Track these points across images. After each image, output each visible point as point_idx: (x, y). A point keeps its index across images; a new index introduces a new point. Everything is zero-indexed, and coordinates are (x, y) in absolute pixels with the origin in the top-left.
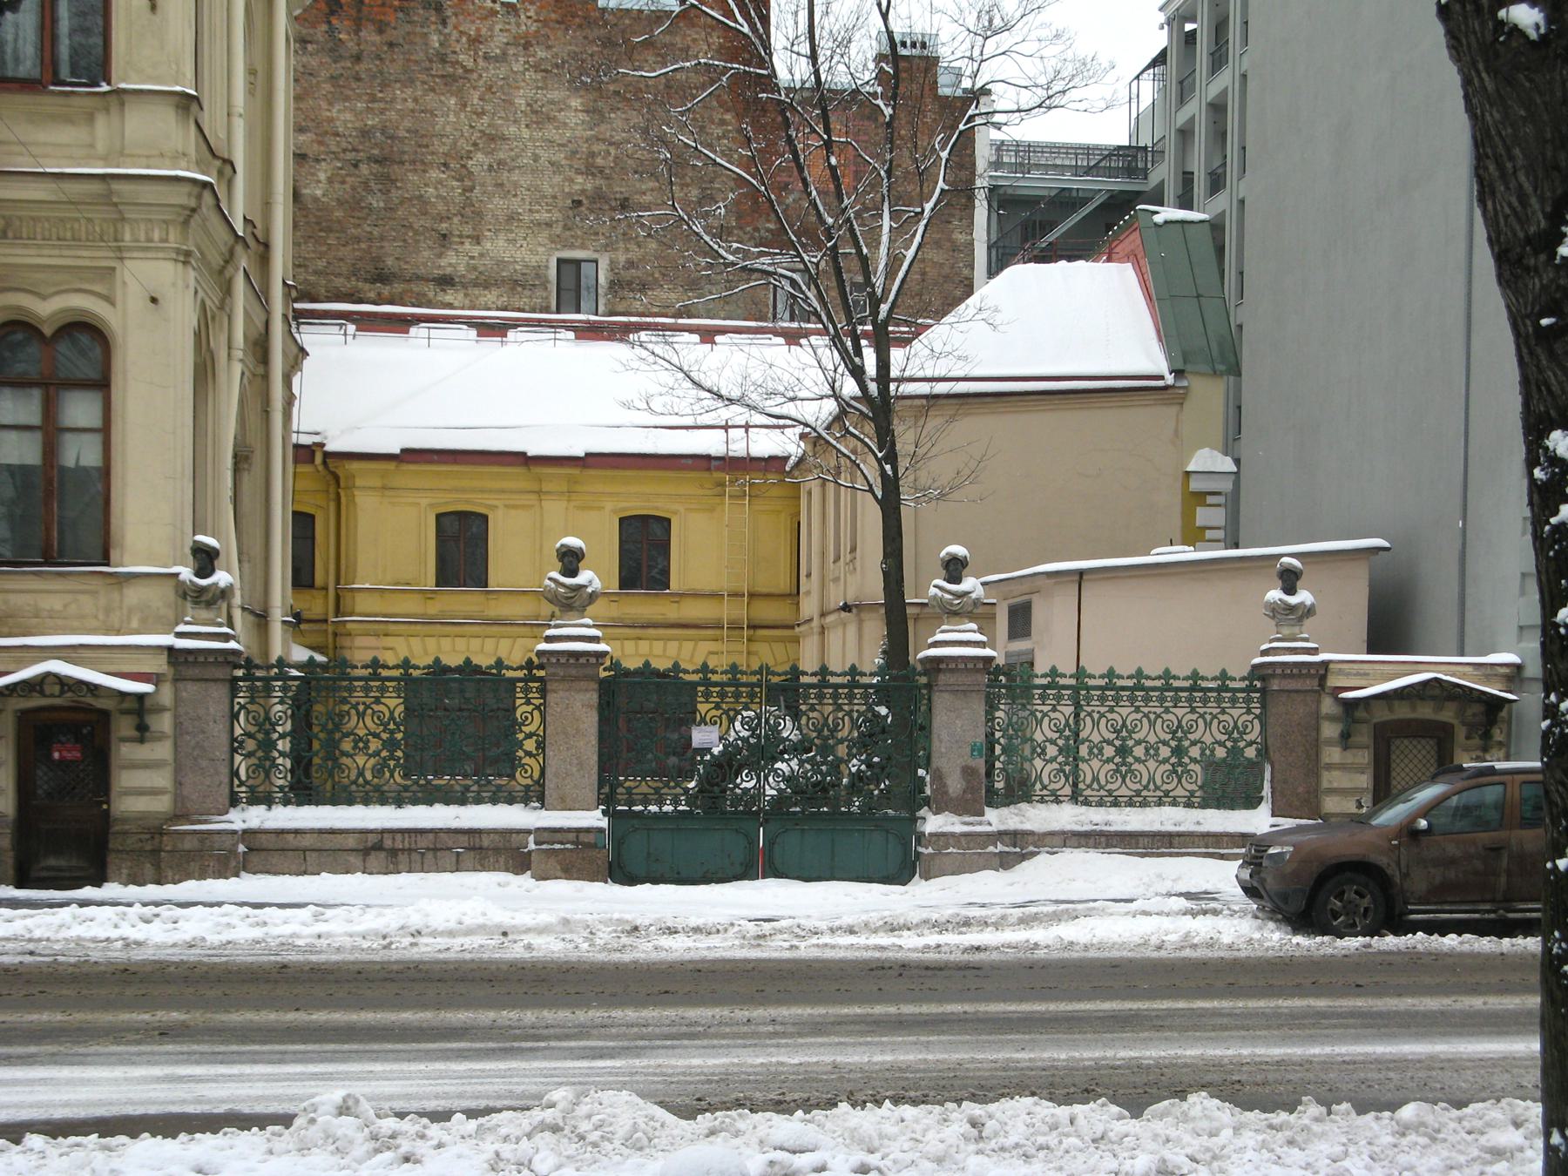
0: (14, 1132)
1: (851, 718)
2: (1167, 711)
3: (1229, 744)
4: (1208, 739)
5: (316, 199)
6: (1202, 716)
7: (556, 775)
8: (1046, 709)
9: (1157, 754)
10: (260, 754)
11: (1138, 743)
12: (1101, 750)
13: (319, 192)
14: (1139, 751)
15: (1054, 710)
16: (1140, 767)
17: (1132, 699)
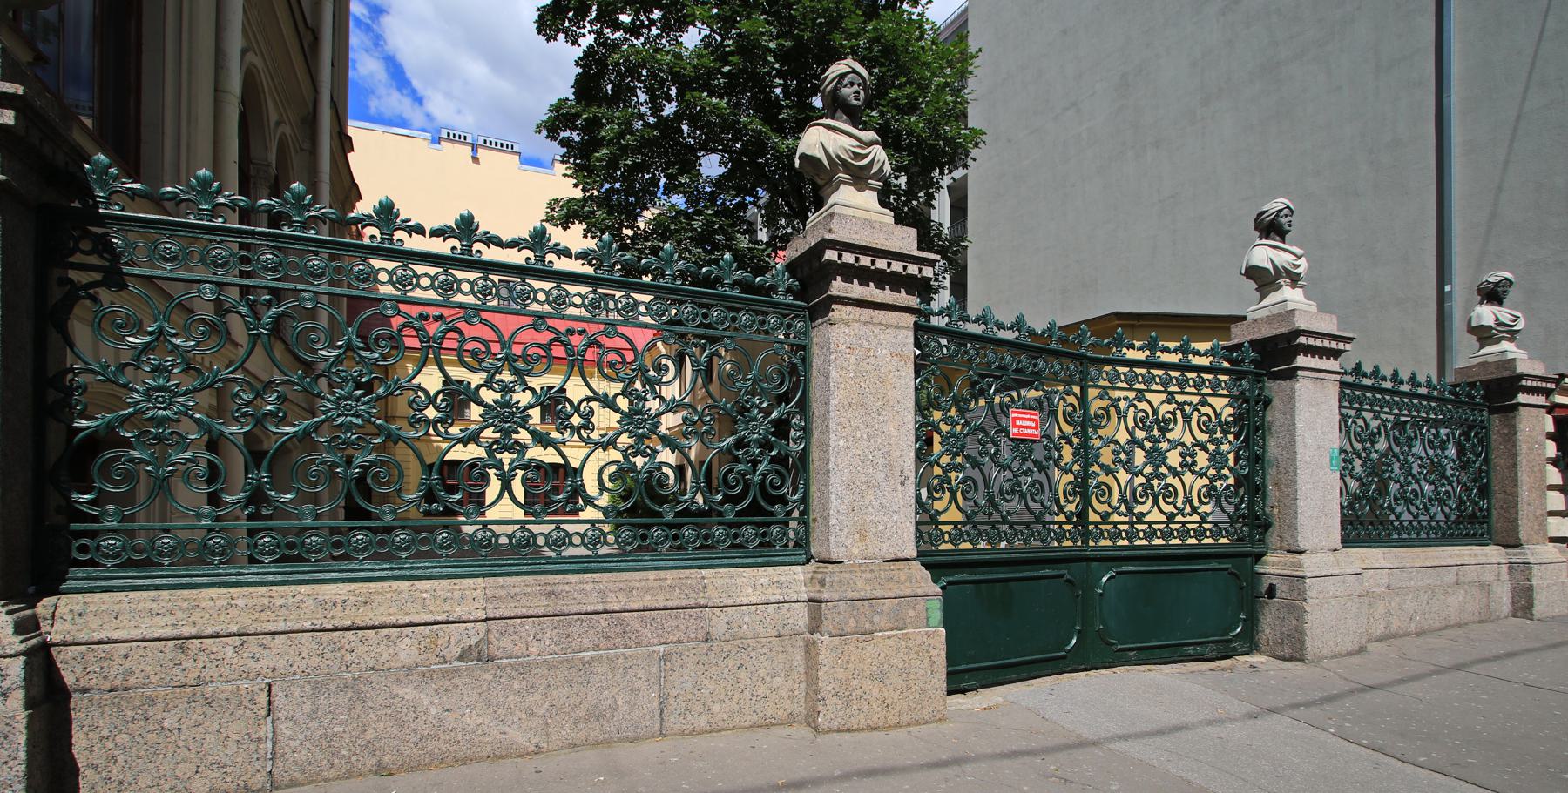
9: (588, 426)
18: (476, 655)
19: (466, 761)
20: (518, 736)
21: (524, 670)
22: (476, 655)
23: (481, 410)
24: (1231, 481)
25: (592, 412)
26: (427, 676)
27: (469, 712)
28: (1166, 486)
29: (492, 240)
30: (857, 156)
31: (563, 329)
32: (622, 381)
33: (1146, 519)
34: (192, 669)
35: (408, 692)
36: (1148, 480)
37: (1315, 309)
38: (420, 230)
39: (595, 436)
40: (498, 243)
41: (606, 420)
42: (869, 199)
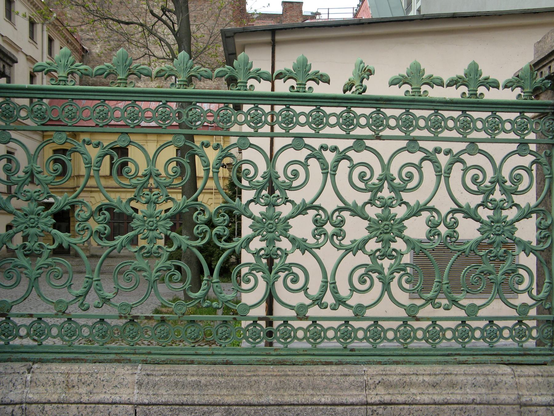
1: (335, 292)
2: (360, 144)
3: (485, 213)
4: (443, 204)
5: (96, 53)
9: (340, 234)
11: (303, 209)
13: (97, 51)
14: (356, 228)
16: (307, 260)
23: (250, 221)
24: (407, 259)
25: (456, 223)
29: (433, 82)
31: (431, 150)
32: (483, 193)
33: (369, 313)
38: (496, 85)
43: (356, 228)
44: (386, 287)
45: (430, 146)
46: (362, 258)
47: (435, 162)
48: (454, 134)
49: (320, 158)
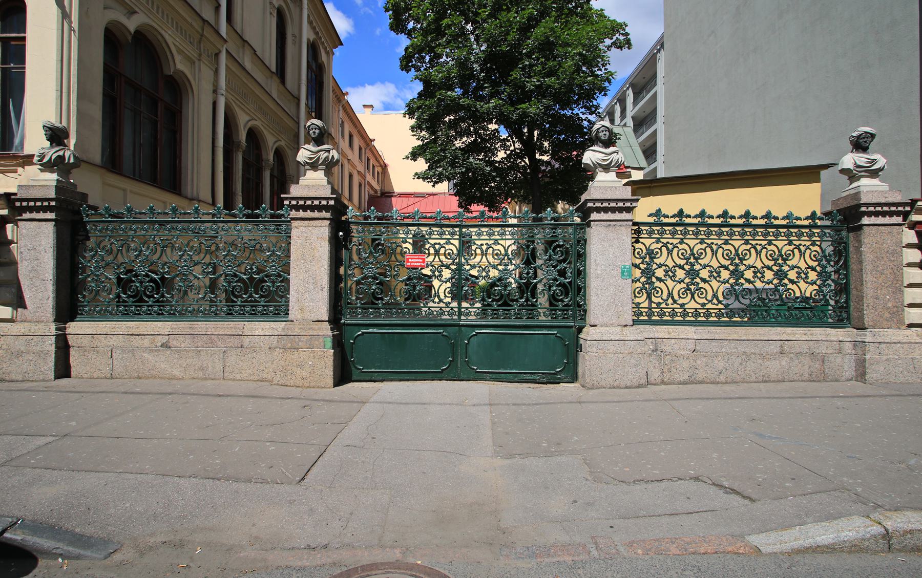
0: (917, 549)
6: (797, 247)
7: (297, 291)
8: (675, 241)
10: (732, 281)
12: (719, 273)
14: (680, 274)
15: (681, 242)
17: (743, 235)
18: (165, 346)
19: (161, 378)
20: (177, 373)
21: (178, 352)
22: (165, 346)
24: (833, 287)
26: (151, 351)
27: (163, 363)
28: (743, 290)
30: (310, 159)
34: (96, 343)
35: (146, 355)
36: (688, 285)
37: (887, 188)
38: (667, 217)
39: (677, 279)
40: (667, 217)
41: (704, 274)
42: (612, 176)
43: (704, 274)
44: (693, 297)
45: (797, 243)
46: (728, 286)
47: (667, 247)
48: (806, 238)
49: (755, 248)
